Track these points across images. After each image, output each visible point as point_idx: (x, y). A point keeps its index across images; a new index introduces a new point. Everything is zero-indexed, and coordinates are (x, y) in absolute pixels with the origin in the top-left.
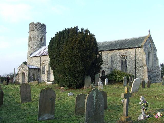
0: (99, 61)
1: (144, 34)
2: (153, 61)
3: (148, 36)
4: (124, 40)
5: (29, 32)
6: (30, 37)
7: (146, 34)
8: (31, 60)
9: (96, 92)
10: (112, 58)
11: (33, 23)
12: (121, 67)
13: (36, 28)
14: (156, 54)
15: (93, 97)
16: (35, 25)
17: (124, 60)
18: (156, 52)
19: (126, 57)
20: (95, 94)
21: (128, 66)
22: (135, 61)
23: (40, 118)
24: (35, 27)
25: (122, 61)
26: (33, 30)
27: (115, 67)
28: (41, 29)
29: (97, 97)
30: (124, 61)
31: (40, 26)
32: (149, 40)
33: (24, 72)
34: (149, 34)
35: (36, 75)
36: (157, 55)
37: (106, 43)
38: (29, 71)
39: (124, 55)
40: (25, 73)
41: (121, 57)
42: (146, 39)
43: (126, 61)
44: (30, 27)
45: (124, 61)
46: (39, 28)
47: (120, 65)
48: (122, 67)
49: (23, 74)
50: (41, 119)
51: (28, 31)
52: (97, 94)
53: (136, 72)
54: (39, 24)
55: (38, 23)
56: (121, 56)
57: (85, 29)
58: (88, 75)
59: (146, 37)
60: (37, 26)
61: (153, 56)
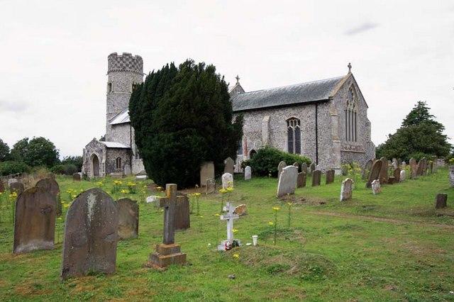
0: (237, 133)
1: (330, 71)
2: (358, 128)
3: (346, 76)
4: (284, 90)
5: (108, 73)
6: (110, 85)
7: (344, 73)
8: (113, 131)
9: (94, 194)
10: (269, 126)
11: (116, 54)
12: (289, 143)
13: (122, 65)
14: (366, 115)
15: (87, 205)
16: (119, 60)
17: (293, 128)
18: (366, 111)
19: (299, 122)
20: (92, 200)
21: (302, 142)
22: (317, 129)
23: (17, 248)
24: (119, 62)
25: (290, 130)
26: (116, 68)
27: (277, 142)
28: (133, 66)
29: (97, 205)
30: (294, 129)
31: (130, 60)
32: (350, 86)
33: (97, 154)
34: (350, 72)
35: (122, 161)
36: (368, 117)
37: (259, 92)
38: (106, 154)
39: (293, 118)
40: (99, 158)
41: (288, 122)
42: (341, 84)
43: (298, 129)
44: (109, 63)
45: (294, 129)
46: (127, 65)
47: (286, 138)
48: (290, 144)
49: (95, 159)
50: (19, 249)
51: (106, 69)
52: (98, 199)
53: (317, 153)
54: (128, 57)
55: (125, 54)
56: (289, 120)
57: (208, 64)
58: (208, 160)
59: (342, 79)
60: (124, 60)
61: (358, 118)
